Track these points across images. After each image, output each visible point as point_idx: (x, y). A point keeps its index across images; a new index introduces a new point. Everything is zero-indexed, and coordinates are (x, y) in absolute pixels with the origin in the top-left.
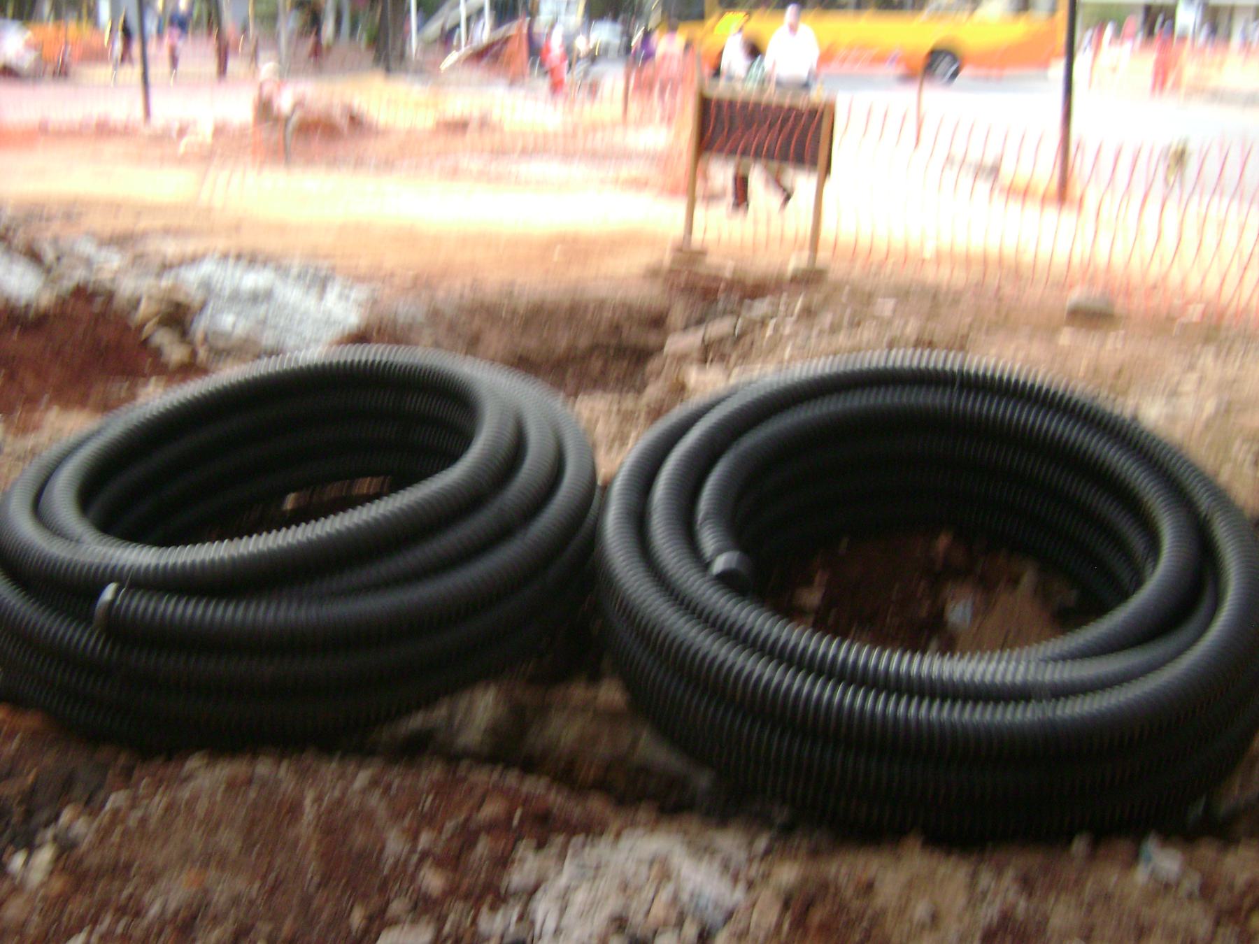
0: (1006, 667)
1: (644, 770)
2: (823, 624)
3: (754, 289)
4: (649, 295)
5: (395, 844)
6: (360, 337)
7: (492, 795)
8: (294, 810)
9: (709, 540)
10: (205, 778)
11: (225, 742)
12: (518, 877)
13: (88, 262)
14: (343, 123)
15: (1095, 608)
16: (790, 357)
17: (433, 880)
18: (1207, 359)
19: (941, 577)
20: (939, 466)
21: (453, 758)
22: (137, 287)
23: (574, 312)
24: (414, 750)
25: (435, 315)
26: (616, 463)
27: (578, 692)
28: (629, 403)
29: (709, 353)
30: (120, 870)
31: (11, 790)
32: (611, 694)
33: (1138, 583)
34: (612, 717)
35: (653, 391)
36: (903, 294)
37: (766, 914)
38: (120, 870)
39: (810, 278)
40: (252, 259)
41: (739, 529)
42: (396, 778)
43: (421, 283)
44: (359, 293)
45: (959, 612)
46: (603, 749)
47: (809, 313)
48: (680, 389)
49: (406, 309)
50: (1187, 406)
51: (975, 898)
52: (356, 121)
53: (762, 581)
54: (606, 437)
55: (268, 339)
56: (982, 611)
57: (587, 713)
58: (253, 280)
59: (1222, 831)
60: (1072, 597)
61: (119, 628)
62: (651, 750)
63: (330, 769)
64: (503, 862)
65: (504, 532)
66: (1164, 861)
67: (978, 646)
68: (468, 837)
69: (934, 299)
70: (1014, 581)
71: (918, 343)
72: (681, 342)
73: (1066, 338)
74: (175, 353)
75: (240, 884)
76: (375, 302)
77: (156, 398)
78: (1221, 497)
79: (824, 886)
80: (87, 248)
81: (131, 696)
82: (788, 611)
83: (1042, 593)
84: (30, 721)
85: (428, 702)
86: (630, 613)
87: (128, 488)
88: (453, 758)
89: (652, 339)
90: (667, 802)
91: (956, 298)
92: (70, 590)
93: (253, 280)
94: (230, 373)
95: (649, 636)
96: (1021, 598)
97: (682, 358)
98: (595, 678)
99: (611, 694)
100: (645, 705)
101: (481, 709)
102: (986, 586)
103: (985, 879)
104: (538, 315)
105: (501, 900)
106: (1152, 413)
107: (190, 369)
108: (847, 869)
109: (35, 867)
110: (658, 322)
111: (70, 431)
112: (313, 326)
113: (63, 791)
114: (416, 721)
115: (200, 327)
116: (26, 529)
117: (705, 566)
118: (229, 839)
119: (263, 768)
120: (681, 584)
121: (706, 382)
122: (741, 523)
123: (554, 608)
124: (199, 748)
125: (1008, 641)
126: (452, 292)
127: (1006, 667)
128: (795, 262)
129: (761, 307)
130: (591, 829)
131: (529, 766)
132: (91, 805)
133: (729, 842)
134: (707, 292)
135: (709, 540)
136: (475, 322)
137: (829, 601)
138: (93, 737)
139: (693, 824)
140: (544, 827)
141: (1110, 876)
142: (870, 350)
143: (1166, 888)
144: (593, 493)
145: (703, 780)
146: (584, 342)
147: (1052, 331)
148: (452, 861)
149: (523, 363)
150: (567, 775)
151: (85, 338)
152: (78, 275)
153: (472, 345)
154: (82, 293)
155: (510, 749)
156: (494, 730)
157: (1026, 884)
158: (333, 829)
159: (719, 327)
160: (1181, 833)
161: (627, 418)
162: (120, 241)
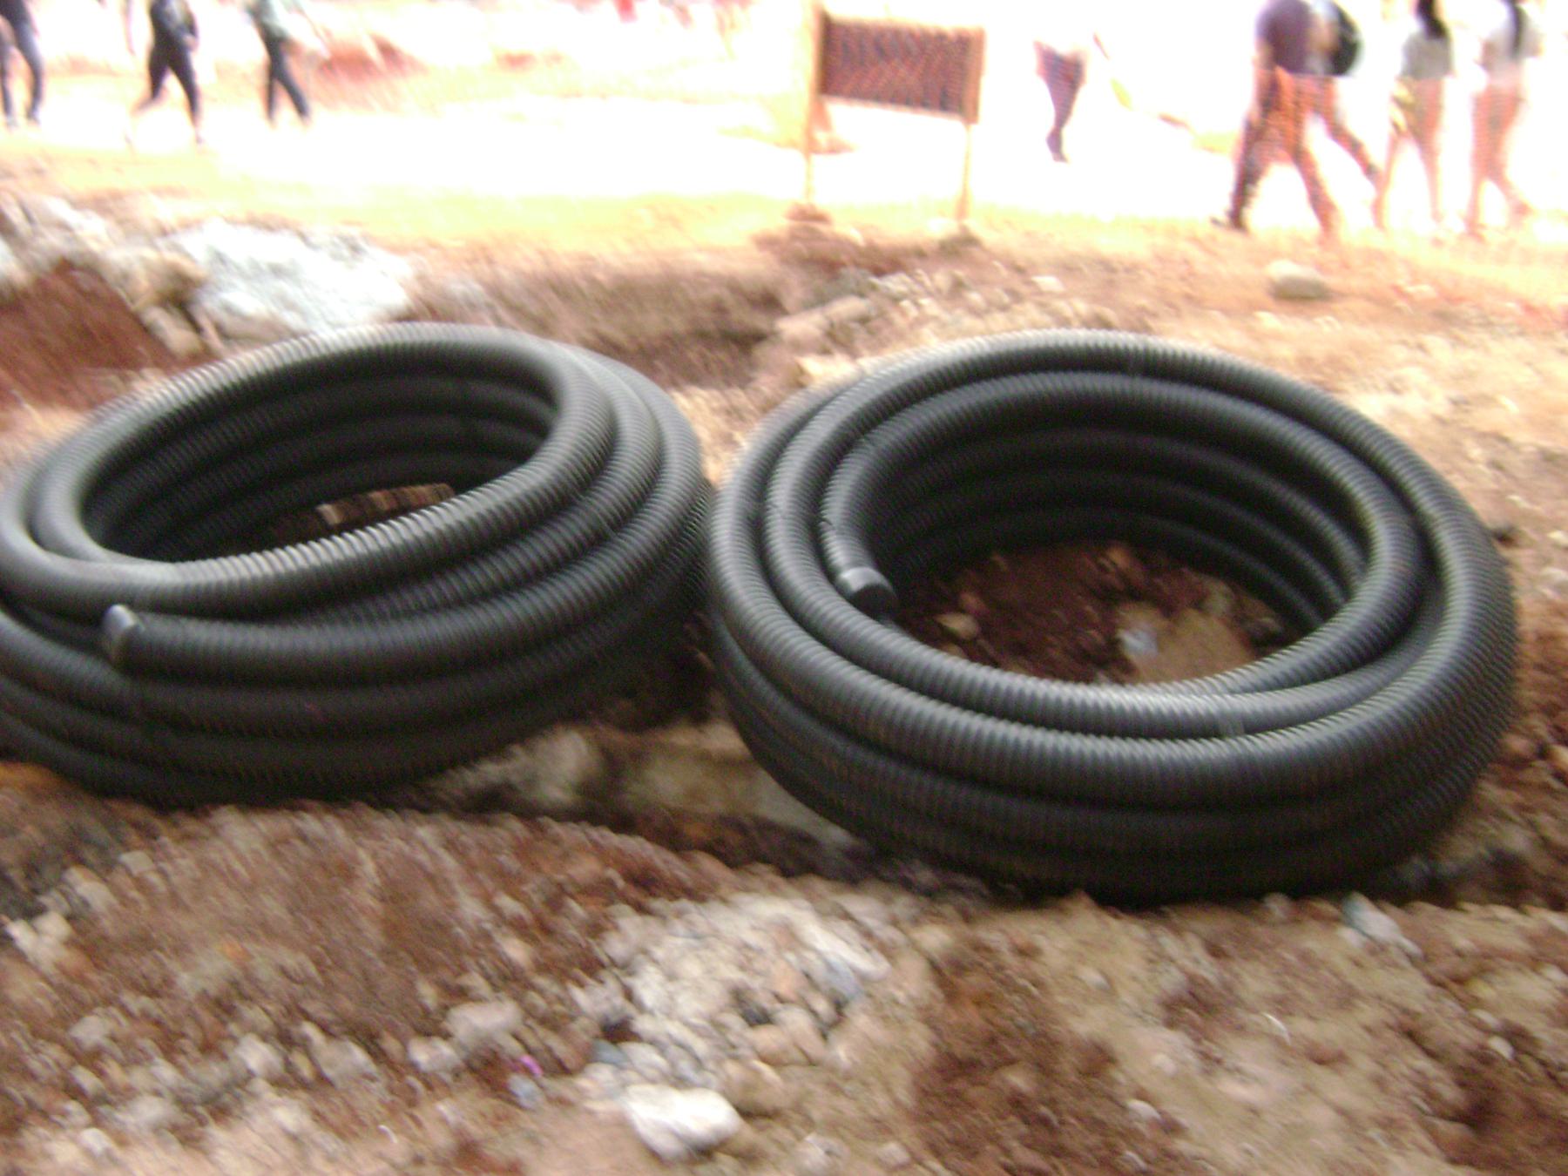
0: (1195, 697)
1: (766, 826)
2: (973, 652)
3: (885, 261)
4: (754, 266)
5: (471, 909)
6: (408, 317)
7: (586, 854)
8: (347, 872)
9: (840, 550)
10: (241, 836)
11: (264, 793)
12: (615, 946)
13: (64, 226)
14: (373, 53)
15: (1295, 629)
16: (939, 336)
17: (516, 951)
18: (1437, 343)
19: (1114, 596)
20: (1100, 483)
21: (530, 813)
22: (127, 258)
23: (666, 288)
24: (488, 805)
25: (496, 291)
26: (726, 469)
27: (683, 737)
28: (739, 397)
29: (837, 340)
30: (144, 942)
31: (6, 854)
32: (724, 739)
33: (1348, 594)
34: (725, 764)
35: (766, 384)
36: (1067, 268)
37: (913, 983)
38: (144, 942)
39: (959, 248)
40: (266, 225)
41: (878, 540)
42: (469, 834)
43: (481, 254)
44: (404, 268)
45: (1137, 638)
46: (716, 805)
47: (958, 286)
48: (798, 381)
49: (460, 285)
50: (1413, 404)
51: (1157, 958)
52: (387, 51)
53: (908, 600)
54: (713, 438)
55: (292, 320)
56: (1160, 641)
57: (693, 763)
58: (280, 248)
59: (1442, 893)
60: (1270, 622)
61: (139, 661)
62: (777, 806)
63: (387, 824)
64: (596, 929)
65: (596, 541)
66: (1375, 921)
67: (1158, 676)
68: (555, 903)
69: (1109, 274)
70: (1199, 603)
71: (1087, 324)
72: (798, 326)
73: (1269, 321)
74: (175, 334)
75: (292, 960)
76: (422, 278)
77: (156, 393)
78: (1449, 501)
79: (980, 947)
80: (61, 210)
81: (156, 744)
82: (938, 638)
83: (1237, 619)
84: (25, 774)
85: (496, 749)
86: (746, 637)
87: (144, 494)
88: (530, 813)
89: (759, 321)
90: (794, 862)
91: (1132, 268)
92: (74, 615)
93: (280, 248)
94: (244, 363)
95: (767, 662)
96: (1209, 626)
97: (799, 347)
98: (700, 718)
99: (724, 739)
100: (769, 750)
101: (564, 759)
102: (1168, 609)
103: (1169, 943)
104: (623, 294)
105: (593, 967)
106: (1369, 404)
107: (203, 356)
108: (1005, 932)
109: (43, 939)
110: (770, 302)
111: (61, 435)
112: (345, 307)
113: (73, 851)
114: (491, 771)
115: (209, 305)
116: (22, 545)
117: (830, 573)
118: (274, 907)
119: (311, 823)
120: (805, 602)
121: (827, 371)
122: (880, 532)
123: (653, 637)
124: (225, 802)
125: (1195, 670)
126: (518, 263)
127: (1195, 697)
128: (939, 229)
129: (895, 283)
130: (698, 894)
131: (624, 823)
132: (105, 869)
133: (865, 906)
134: (827, 263)
135: (840, 550)
136: (555, 296)
137: (986, 627)
138: (104, 790)
139: (819, 885)
140: (645, 887)
141: (1313, 940)
142: (1026, 330)
143: (1376, 949)
144: (701, 493)
145: (835, 836)
146: (679, 324)
147: (1252, 307)
148: (537, 930)
149: (608, 348)
150: (671, 837)
151: (69, 323)
152: (53, 242)
153: (543, 327)
154: (65, 267)
155: (602, 805)
156: (586, 789)
157: (1215, 951)
158: (394, 894)
159: (847, 307)
160: (1392, 895)
161: (733, 414)
162: (101, 204)
